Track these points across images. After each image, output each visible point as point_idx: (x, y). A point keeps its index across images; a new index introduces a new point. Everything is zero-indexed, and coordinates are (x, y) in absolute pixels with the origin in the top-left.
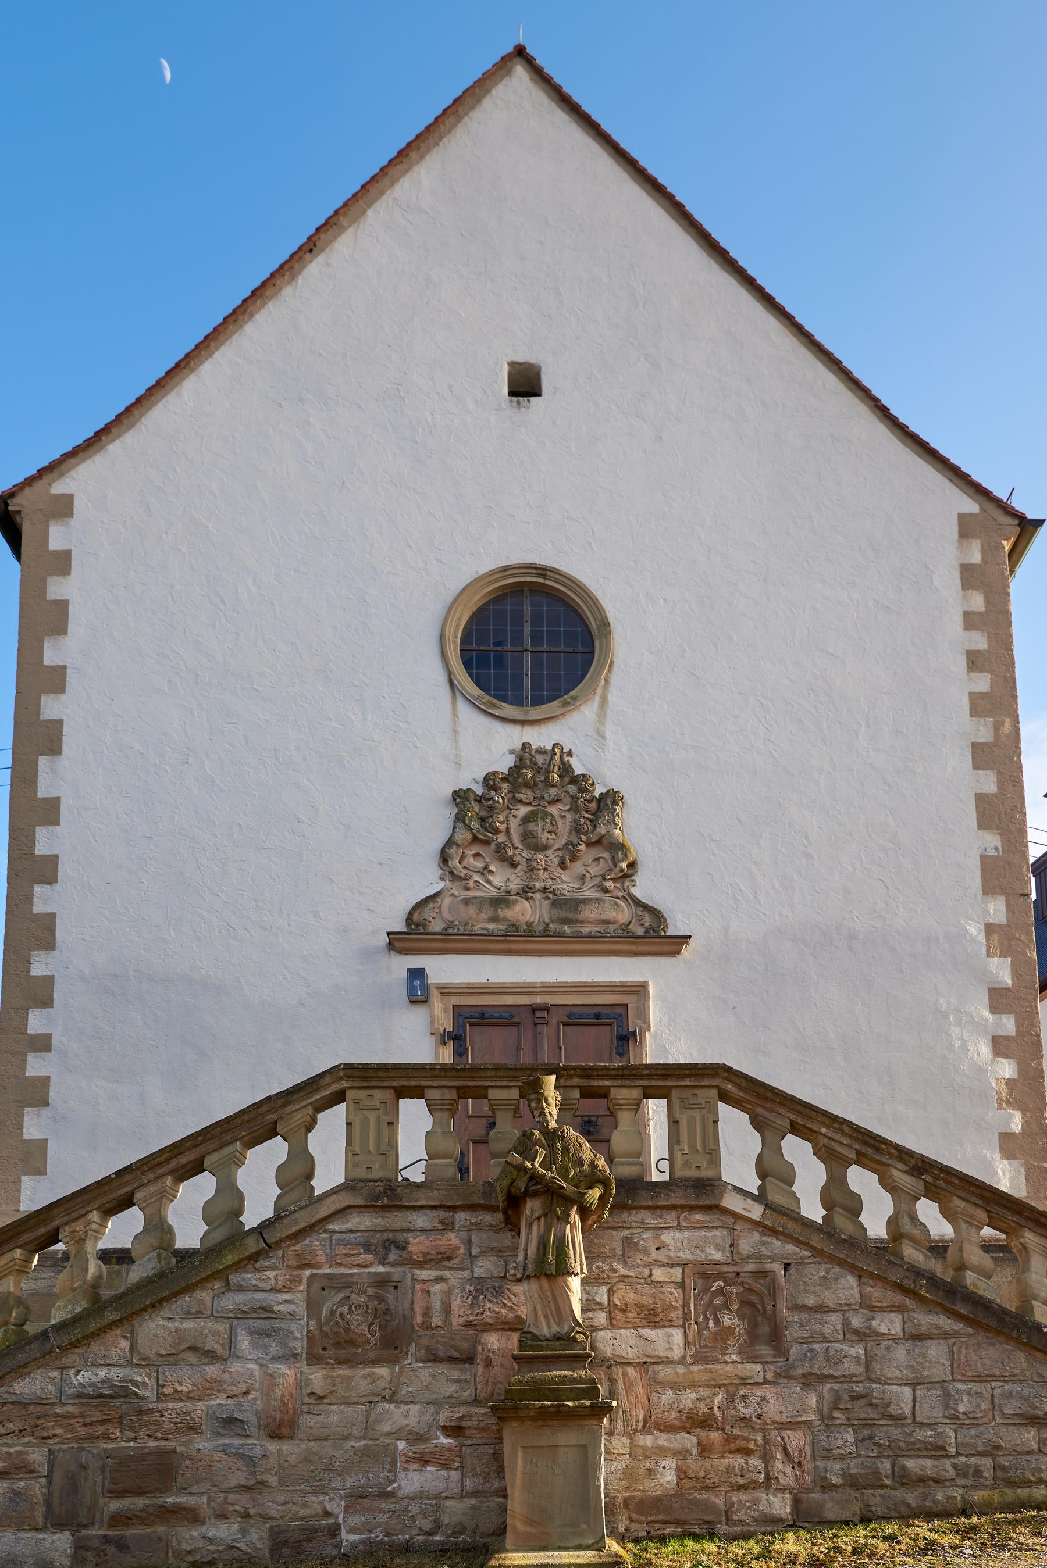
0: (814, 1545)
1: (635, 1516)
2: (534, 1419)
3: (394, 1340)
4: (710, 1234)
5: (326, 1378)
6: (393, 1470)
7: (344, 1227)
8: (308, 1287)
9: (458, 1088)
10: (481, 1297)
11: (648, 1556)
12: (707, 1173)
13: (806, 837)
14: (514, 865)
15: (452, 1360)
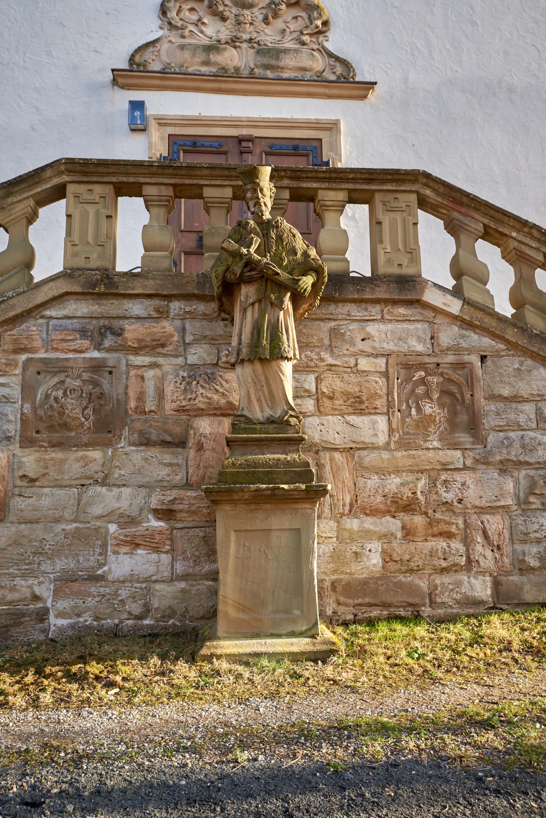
0: (523, 629)
1: (342, 599)
2: (248, 502)
3: (107, 422)
4: (411, 327)
5: (38, 460)
6: (104, 553)
7: (61, 313)
8: (24, 370)
9: (174, 186)
10: (194, 383)
11: (360, 642)
12: (407, 271)
13: (472, 8)
14: (224, 19)
15: (164, 444)
